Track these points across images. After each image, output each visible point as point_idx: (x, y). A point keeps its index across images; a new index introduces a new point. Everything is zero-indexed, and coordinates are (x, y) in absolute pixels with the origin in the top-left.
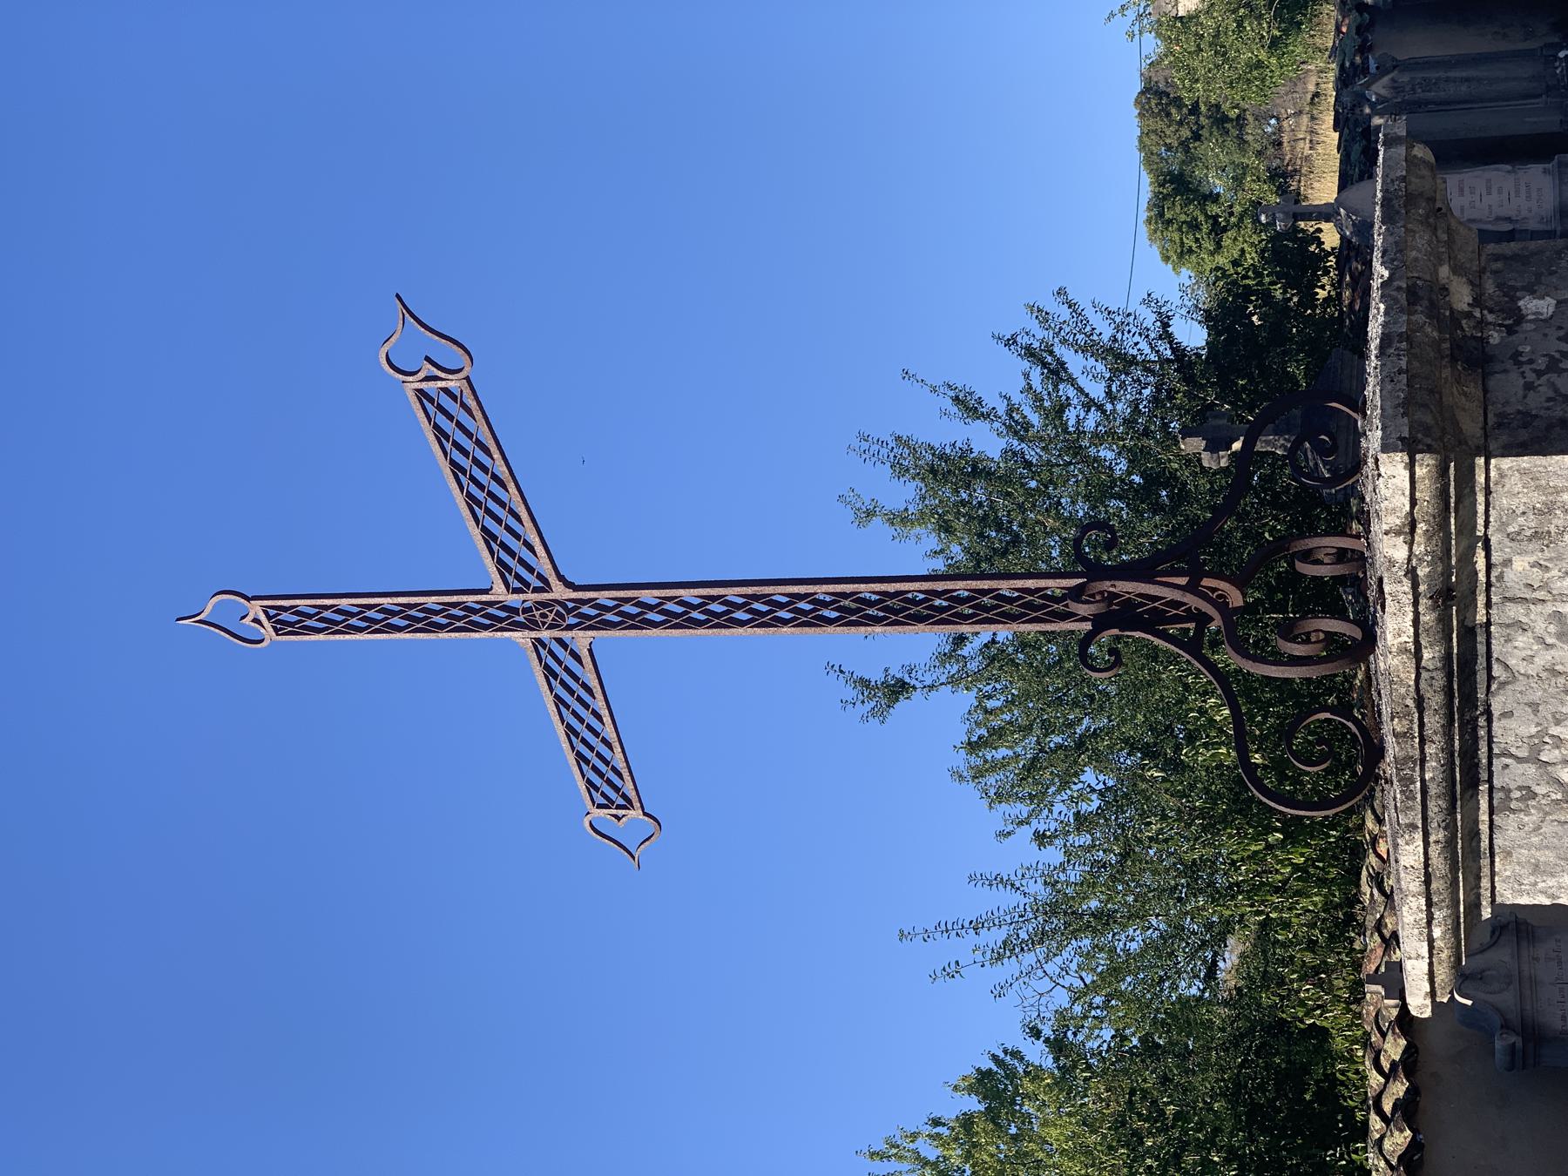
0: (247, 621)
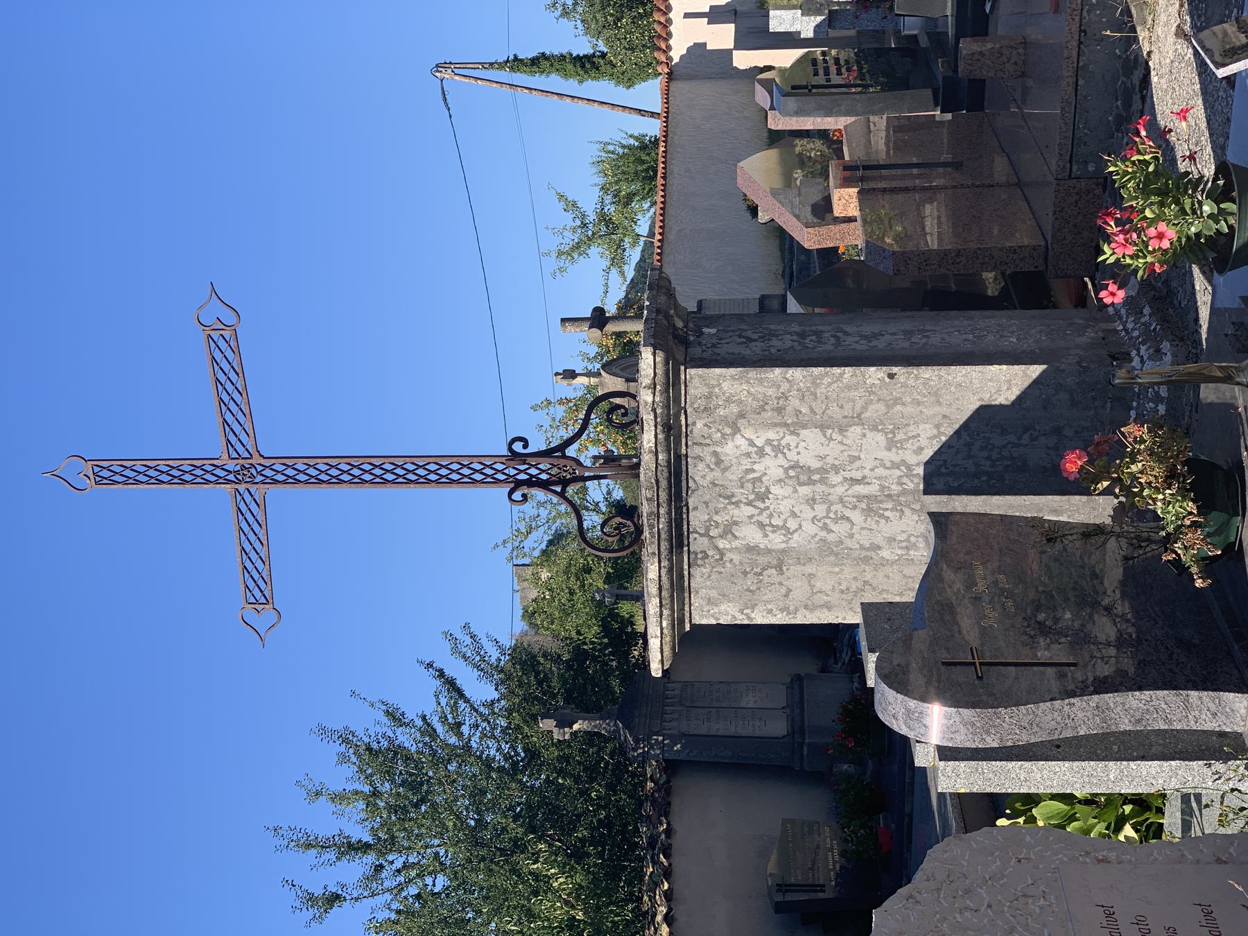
0: (81, 475)
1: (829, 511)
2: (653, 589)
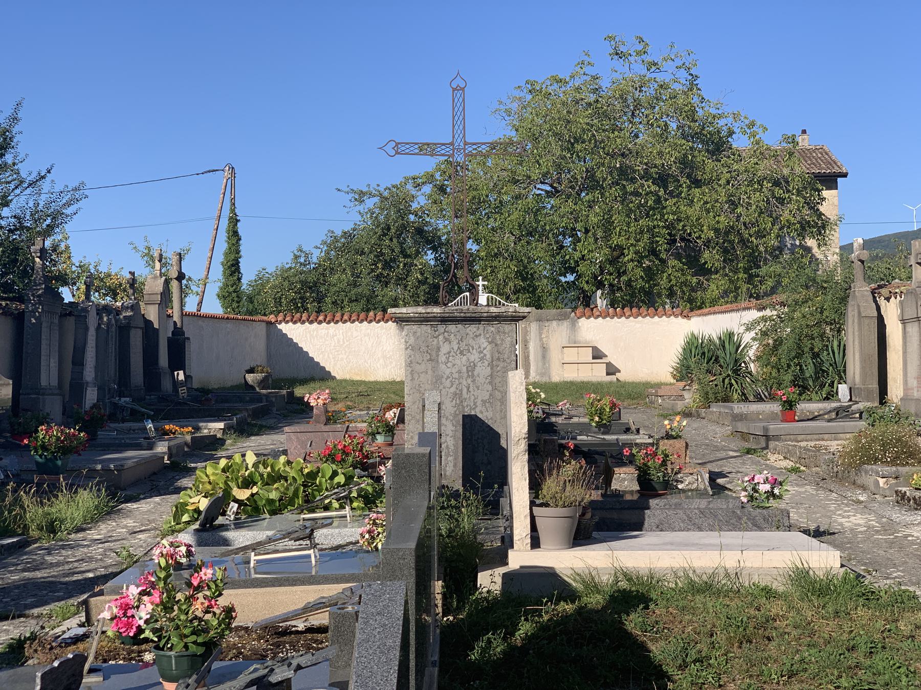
1: (456, 379)
2: (429, 310)
